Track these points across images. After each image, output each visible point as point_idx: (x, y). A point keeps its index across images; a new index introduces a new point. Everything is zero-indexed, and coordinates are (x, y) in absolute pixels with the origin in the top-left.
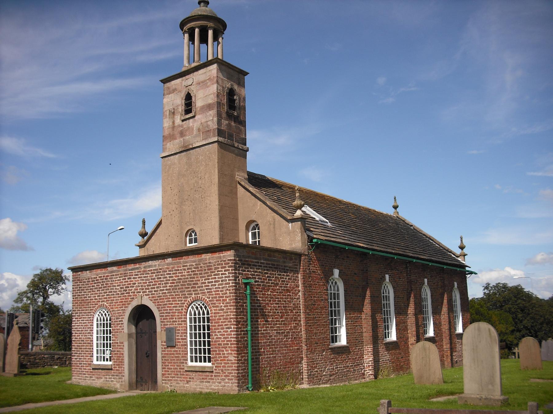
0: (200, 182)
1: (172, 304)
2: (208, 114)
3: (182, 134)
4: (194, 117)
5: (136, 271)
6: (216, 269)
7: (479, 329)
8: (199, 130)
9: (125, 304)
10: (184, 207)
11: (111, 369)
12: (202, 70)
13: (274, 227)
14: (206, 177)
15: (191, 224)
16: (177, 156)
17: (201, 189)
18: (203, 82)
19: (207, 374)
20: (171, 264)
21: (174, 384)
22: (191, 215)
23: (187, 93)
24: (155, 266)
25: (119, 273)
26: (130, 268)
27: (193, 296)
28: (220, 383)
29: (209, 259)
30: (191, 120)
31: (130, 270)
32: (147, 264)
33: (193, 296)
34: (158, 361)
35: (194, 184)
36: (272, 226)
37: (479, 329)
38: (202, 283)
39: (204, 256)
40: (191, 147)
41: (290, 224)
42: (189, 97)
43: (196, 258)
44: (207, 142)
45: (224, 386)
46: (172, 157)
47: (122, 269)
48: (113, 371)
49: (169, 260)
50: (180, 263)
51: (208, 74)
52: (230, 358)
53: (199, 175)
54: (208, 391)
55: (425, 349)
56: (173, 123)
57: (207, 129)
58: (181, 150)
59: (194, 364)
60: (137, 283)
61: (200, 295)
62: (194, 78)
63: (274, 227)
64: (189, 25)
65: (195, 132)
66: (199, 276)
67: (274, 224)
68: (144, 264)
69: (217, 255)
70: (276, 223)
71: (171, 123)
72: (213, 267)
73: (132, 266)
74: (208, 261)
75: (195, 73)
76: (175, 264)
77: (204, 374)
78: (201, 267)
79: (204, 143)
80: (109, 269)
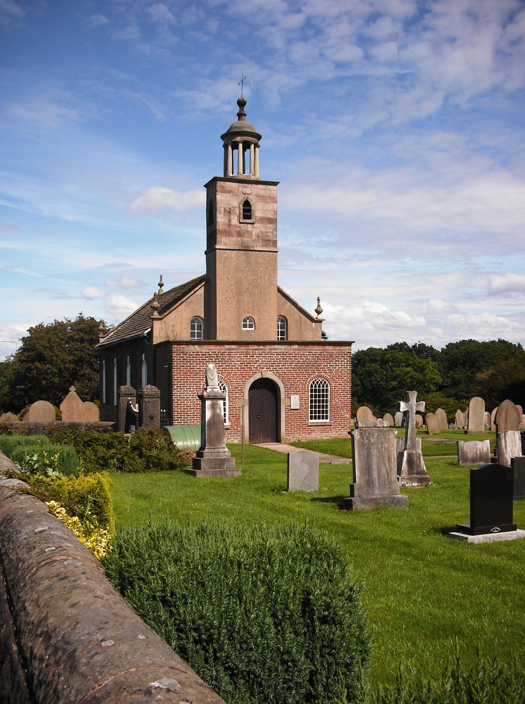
0: (260, 280)
1: (296, 379)
2: (268, 226)
3: (240, 234)
4: (253, 224)
5: (260, 351)
6: (336, 357)
7: (477, 400)
8: (258, 236)
9: (245, 377)
10: (242, 297)
11: (229, 429)
12: (261, 185)
13: (300, 324)
14: (266, 277)
15: (250, 313)
16: (234, 252)
17: (260, 286)
18: (262, 197)
19: (327, 427)
20: (298, 349)
21: (297, 435)
22: (250, 305)
23: (245, 200)
24: (281, 349)
25: (239, 351)
26: (253, 348)
27: (317, 374)
28: (337, 432)
29: (332, 350)
30: (250, 226)
31: (252, 350)
32: (273, 347)
33: (317, 374)
34: (282, 420)
35: (253, 281)
36: (298, 323)
37: (477, 400)
38: (324, 366)
39: (327, 347)
40: (252, 249)
41: (314, 324)
42: (247, 205)
43: (321, 348)
44: (269, 250)
45: (341, 434)
46: (229, 251)
47: (243, 348)
48: (229, 431)
49: (296, 347)
50: (306, 350)
51: (268, 192)
52: (345, 416)
53: (259, 275)
54: (327, 438)
55: (364, 411)
56: (230, 221)
57: (267, 239)
58: (240, 248)
59: (313, 421)
60: (260, 360)
61: (323, 374)
62: (253, 190)
63: (300, 324)
64: (245, 137)
65: (254, 237)
66: (322, 361)
67: (300, 321)
68: (268, 347)
69: (338, 348)
70: (302, 320)
71: (226, 221)
72: (335, 356)
73: (256, 347)
74: (330, 351)
75: (254, 185)
76: (301, 350)
77: (325, 427)
78: (324, 355)
79: (266, 250)
80: (226, 346)
